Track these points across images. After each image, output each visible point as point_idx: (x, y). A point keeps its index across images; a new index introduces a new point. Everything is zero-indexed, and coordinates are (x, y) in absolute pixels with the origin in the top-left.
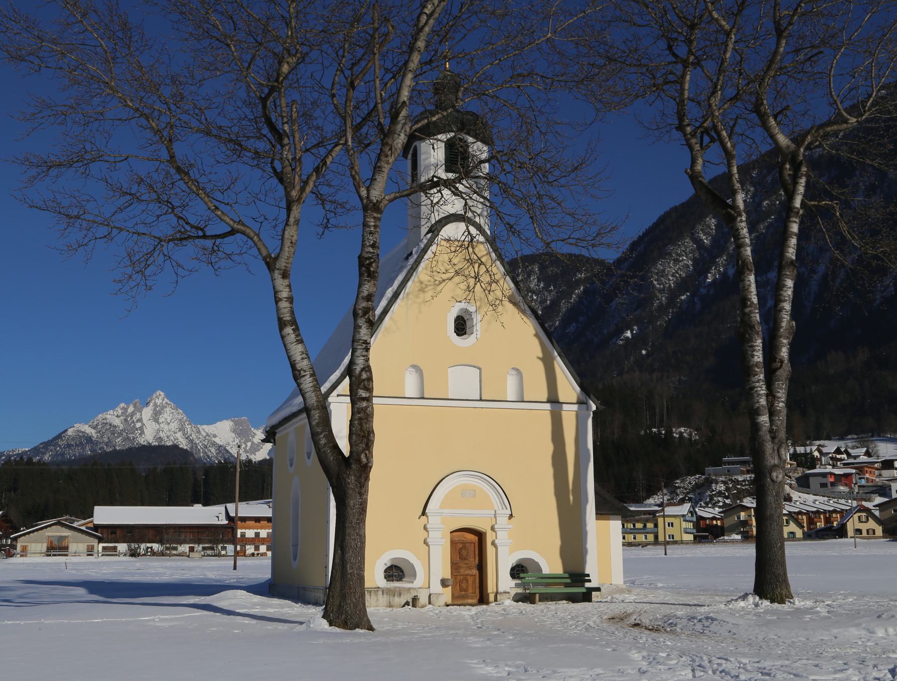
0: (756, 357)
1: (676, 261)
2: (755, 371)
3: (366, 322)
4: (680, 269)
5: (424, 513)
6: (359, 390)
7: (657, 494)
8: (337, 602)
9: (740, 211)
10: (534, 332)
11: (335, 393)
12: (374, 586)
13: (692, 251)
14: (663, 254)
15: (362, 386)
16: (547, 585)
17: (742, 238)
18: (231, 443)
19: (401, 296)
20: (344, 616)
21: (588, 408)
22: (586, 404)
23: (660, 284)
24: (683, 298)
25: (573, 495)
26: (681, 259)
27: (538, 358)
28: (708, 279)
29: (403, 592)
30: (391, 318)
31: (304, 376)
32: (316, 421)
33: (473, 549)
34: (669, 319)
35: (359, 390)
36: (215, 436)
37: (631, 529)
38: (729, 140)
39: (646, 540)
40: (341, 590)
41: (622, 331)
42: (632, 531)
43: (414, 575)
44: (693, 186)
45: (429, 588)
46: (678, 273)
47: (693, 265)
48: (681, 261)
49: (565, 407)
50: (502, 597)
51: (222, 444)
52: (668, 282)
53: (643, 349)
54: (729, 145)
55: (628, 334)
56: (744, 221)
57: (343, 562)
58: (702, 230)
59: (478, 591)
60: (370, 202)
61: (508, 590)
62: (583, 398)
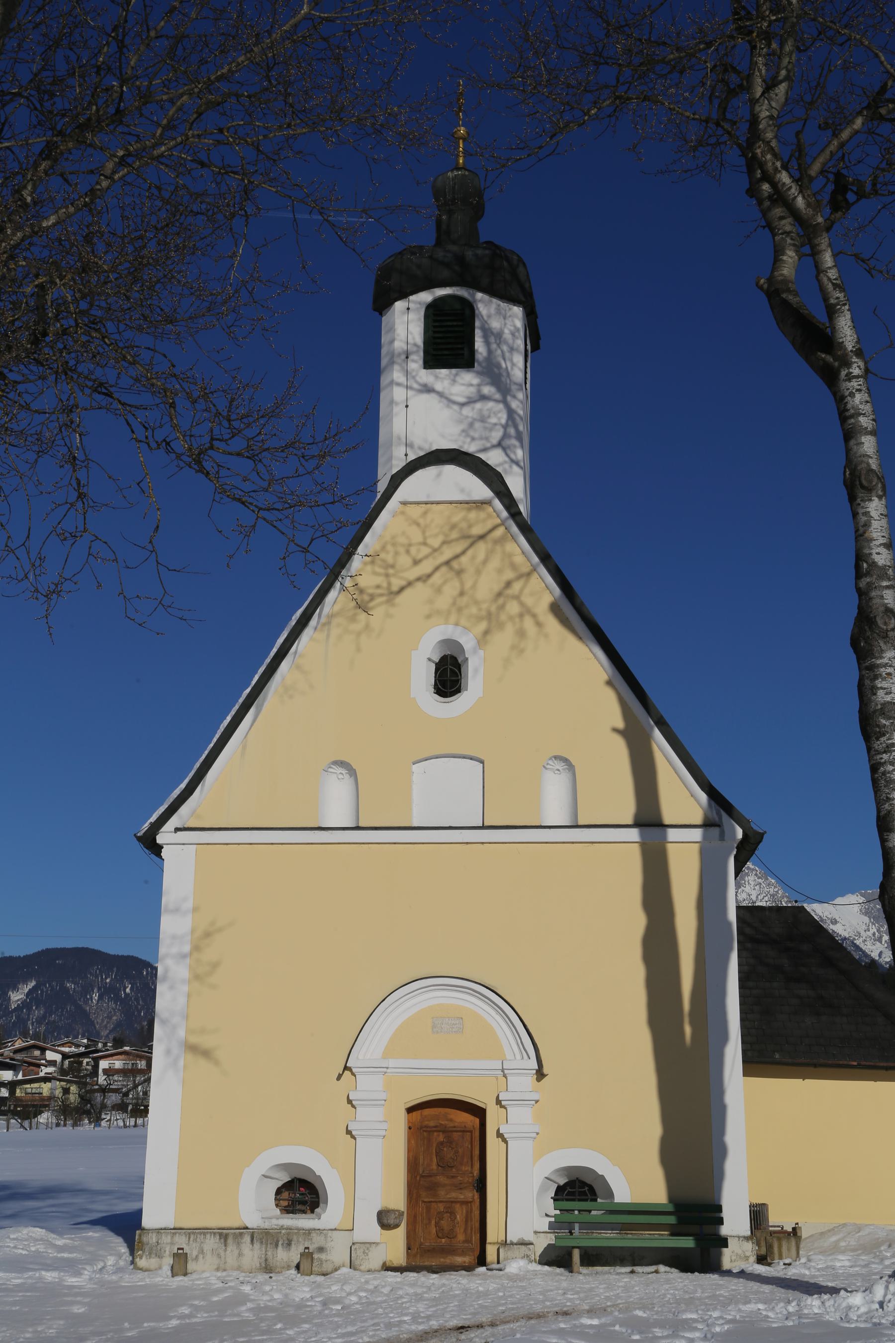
0: (881, 693)
2: (878, 726)
9: (845, 355)
10: (605, 677)
11: (174, 822)
12: (236, 1225)
16: (625, 1227)
17: (852, 416)
18: (863, 933)
19: (313, 622)
22: (719, 826)
25: (692, 1023)
27: (615, 730)
29: (295, 1238)
33: (467, 1145)
36: (834, 922)
38: (801, 192)
44: (772, 311)
49: (673, 834)
50: (510, 1254)
51: (847, 936)
54: (800, 202)
56: (857, 377)
61: (529, 1237)
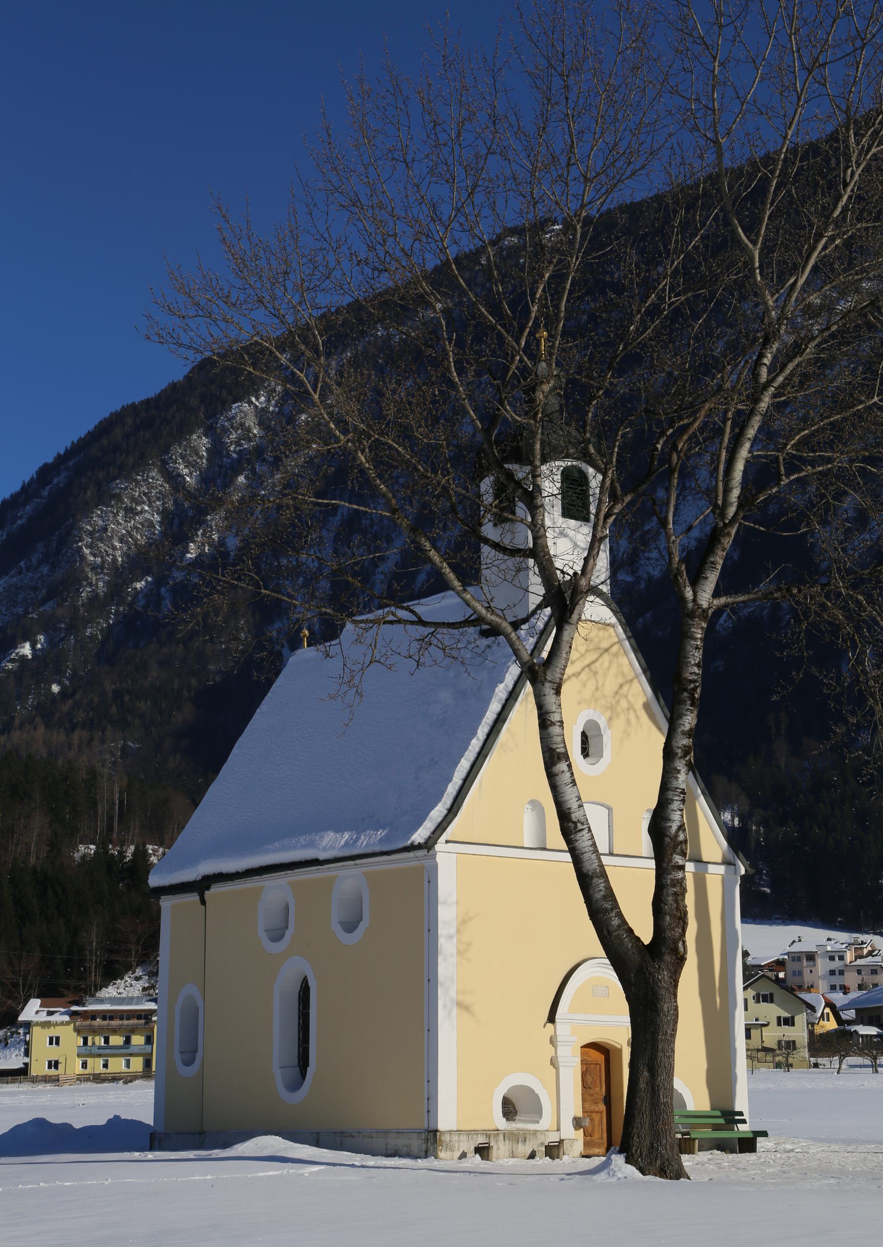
1: (131, 512)
3: (686, 765)
4: (137, 528)
5: (551, 1019)
6: (675, 856)
7: (122, 979)
8: (647, 1142)
12: (492, 1128)
13: (162, 496)
14: (105, 497)
15: (678, 850)
20: (659, 1162)
21: (736, 872)
23: (95, 556)
24: (139, 585)
26: (139, 508)
28: (189, 553)
30: (508, 729)
31: (582, 830)
32: (602, 893)
34: (109, 625)
35: (675, 856)
37: (100, 1048)
39: (127, 1070)
40: (652, 1125)
41: (14, 644)
42: (101, 1052)
43: (537, 1111)
45: (558, 1130)
46: (131, 536)
47: (161, 523)
48: (137, 514)
52: (110, 551)
53: (54, 682)
55: (26, 650)
57: (653, 1087)
58: (182, 457)
59: (605, 1136)
60: (699, 608)
62: (731, 856)
